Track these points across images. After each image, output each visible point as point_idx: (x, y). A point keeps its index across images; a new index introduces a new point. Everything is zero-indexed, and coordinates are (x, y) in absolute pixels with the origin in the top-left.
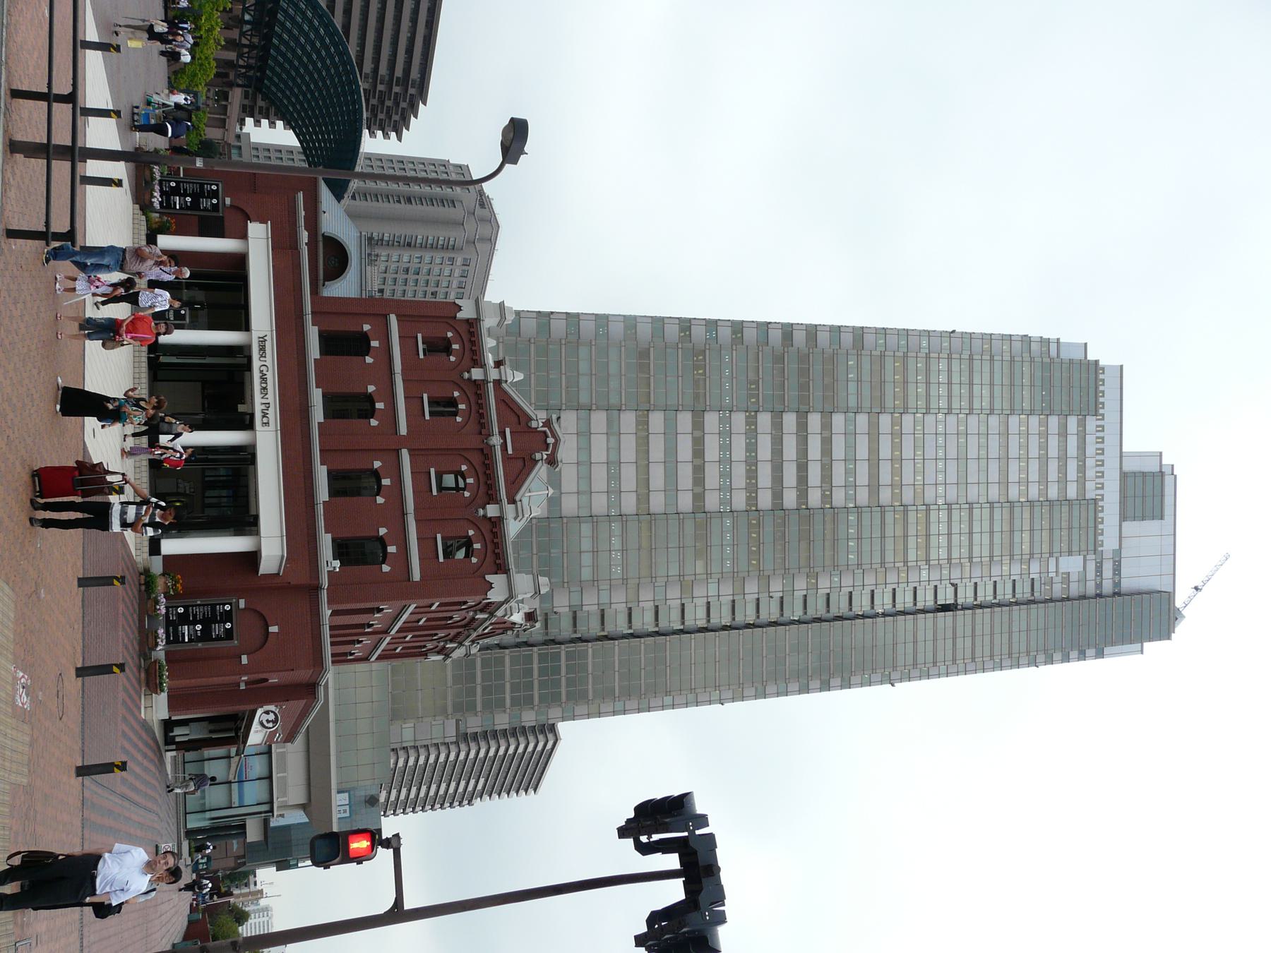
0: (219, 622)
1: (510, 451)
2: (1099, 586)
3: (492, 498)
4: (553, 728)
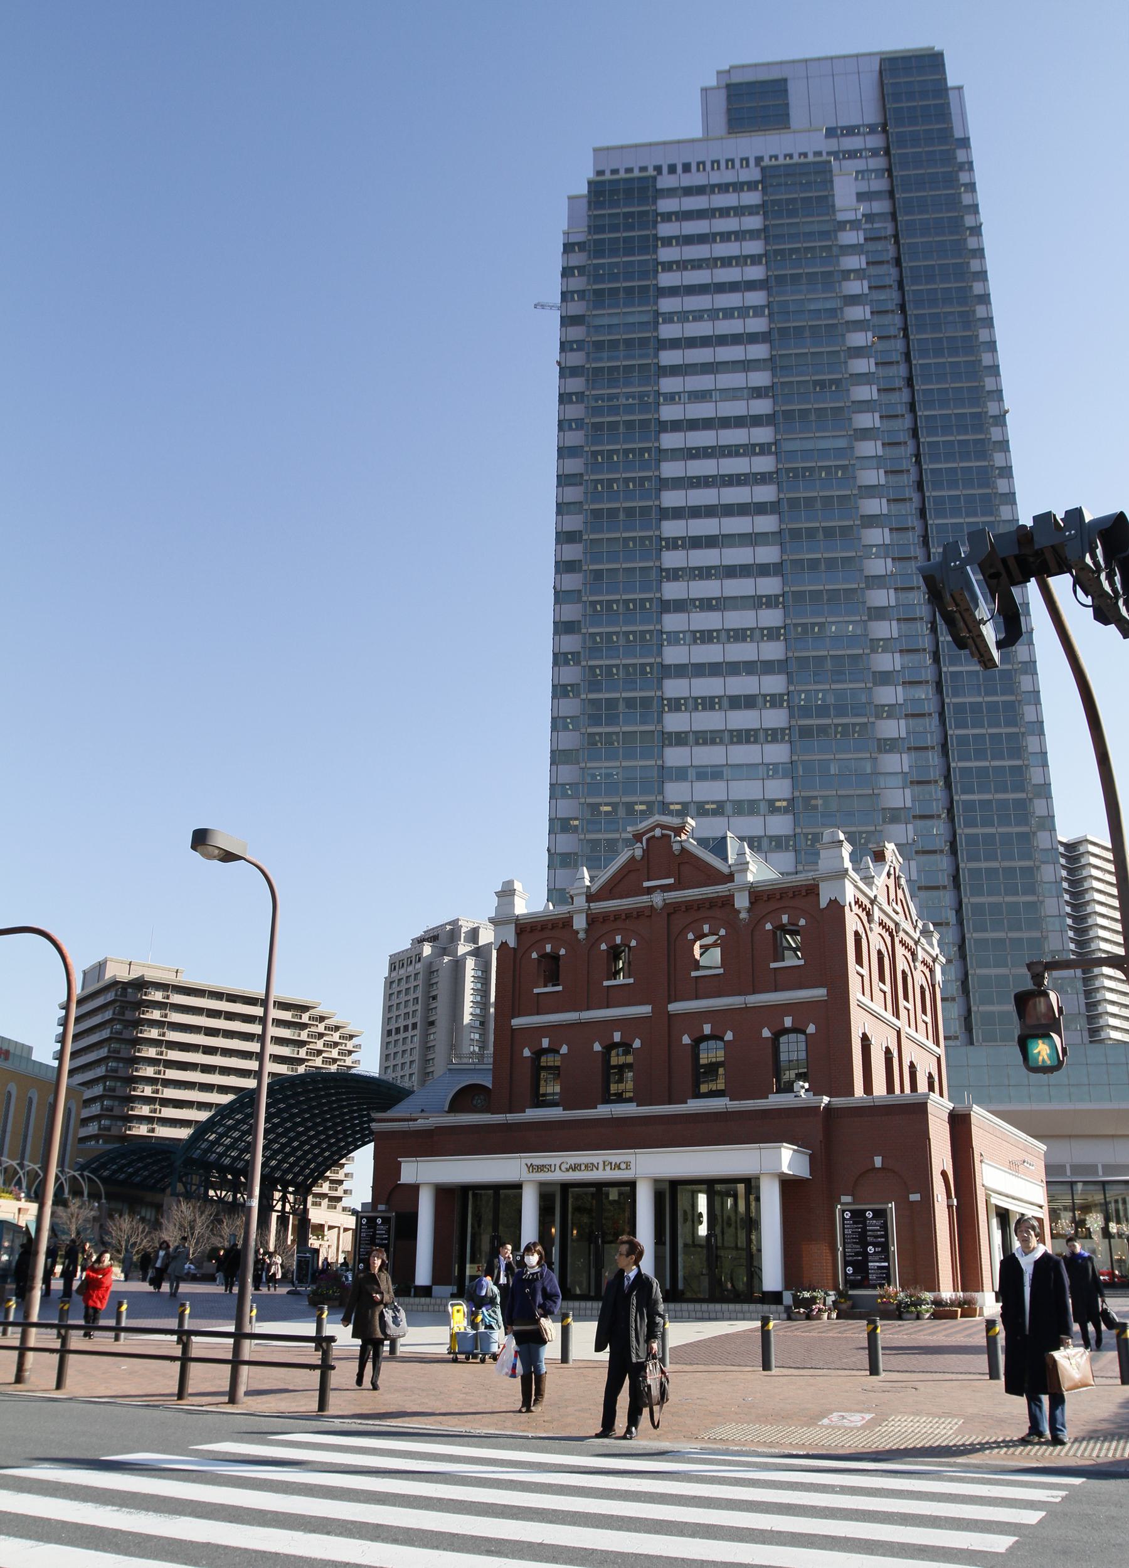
0: (865, 1226)
1: (671, 881)
2: (874, 153)
3: (727, 902)
4: (1071, 847)
